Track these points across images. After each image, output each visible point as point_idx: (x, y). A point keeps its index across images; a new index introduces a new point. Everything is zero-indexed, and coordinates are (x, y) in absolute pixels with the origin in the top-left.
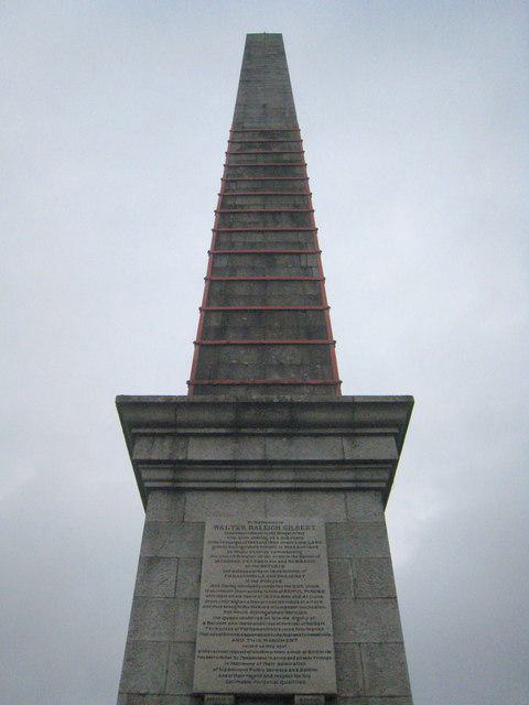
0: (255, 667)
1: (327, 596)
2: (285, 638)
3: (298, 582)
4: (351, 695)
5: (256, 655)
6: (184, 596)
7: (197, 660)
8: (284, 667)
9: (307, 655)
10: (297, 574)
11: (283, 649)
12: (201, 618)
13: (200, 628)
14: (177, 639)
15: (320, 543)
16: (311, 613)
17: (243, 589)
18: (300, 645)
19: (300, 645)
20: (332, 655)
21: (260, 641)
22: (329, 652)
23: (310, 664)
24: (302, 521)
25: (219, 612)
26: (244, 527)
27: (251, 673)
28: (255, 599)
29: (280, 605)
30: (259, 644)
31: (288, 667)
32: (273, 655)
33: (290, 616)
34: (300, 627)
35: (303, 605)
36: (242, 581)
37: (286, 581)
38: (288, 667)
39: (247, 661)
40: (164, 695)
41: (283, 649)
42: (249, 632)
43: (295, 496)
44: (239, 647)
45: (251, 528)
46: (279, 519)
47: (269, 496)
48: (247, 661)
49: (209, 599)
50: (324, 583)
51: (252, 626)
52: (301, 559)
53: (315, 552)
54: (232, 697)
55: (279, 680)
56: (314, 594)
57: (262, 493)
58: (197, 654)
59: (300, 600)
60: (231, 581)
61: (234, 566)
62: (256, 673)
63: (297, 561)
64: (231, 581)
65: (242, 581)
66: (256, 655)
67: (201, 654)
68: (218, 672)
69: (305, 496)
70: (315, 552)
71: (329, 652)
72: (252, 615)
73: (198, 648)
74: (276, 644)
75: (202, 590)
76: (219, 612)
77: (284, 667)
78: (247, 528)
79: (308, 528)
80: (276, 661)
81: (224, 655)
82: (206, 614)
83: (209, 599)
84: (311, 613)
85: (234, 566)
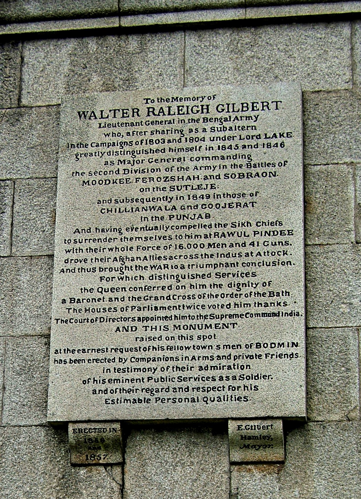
0: (159, 374)
1: (298, 240)
2: (214, 322)
3: (238, 215)
4: (336, 417)
5: (160, 354)
6: (28, 251)
7: (52, 366)
8: (210, 373)
9: (254, 351)
10: (238, 201)
11: (208, 342)
12: (59, 293)
13: (57, 310)
14: (18, 332)
15: (289, 135)
16: (265, 274)
17: (136, 234)
18: (244, 332)
19: (244, 332)
20: (301, 350)
21: (166, 328)
22: (295, 345)
23: (257, 367)
24: (254, 92)
25: (92, 281)
26: (136, 111)
27: (151, 384)
28: (159, 253)
29: (207, 261)
30: (164, 334)
31: (217, 373)
32: (189, 353)
33: (224, 281)
34: (244, 300)
35: (249, 260)
36: (134, 219)
37: (217, 216)
38: (217, 373)
39: (141, 365)
40: (328, 164)
41: (208, 342)
42: (146, 313)
43: (246, 36)
44: (127, 340)
45: (150, 111)
46: (208, 90)
47: (192, 40)
48: (141, 365)
49: (70, 256)
50: (295, 218)
51: (154, 303)
52: (250, 170)
53: (277, 155)
54: (117, 426)
55: (201, 395)
56: (271, 239)
57: (179, 36)
58: (52, 356)
59: (244, 251)
60: (112, 220)
61: (117, 190)
62: (159, 385)
63: (241, 176)
64: (112, 220)
65: (134, 219)
66: (160, 354)
67: (62, 356)
68: (91, 386)
69: (269, 34)
70: (277, 155)
71: (295, 345)
72: (152, 283)
73: (54, 346)
74: (196, 333)
75: (57, 240)
76: (92, 281)
77: (210, 373)
78: (143, 111)
79: (266, 106)
80: (197, 363)
81: (101, 356)
82: (65, 285)
83: (70, 256)
84: (265, 274)
85: (117, 190)
